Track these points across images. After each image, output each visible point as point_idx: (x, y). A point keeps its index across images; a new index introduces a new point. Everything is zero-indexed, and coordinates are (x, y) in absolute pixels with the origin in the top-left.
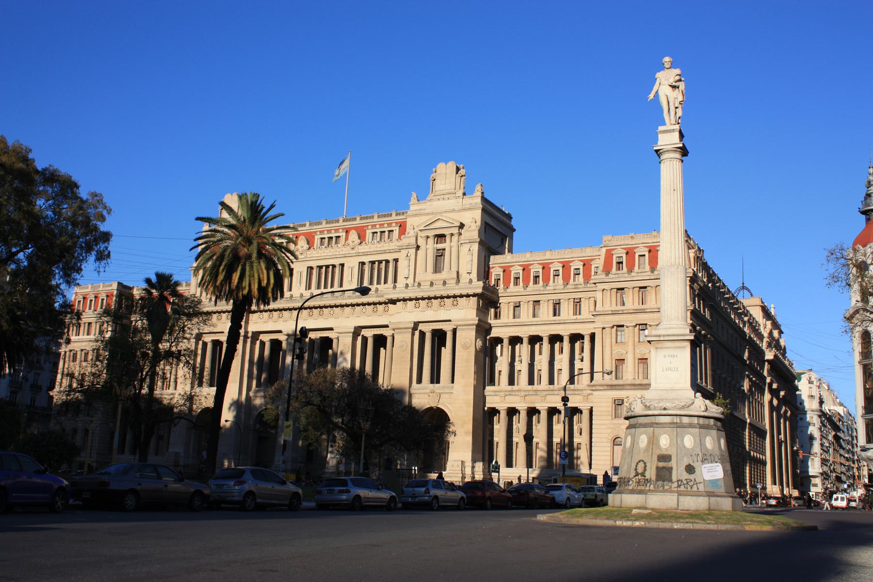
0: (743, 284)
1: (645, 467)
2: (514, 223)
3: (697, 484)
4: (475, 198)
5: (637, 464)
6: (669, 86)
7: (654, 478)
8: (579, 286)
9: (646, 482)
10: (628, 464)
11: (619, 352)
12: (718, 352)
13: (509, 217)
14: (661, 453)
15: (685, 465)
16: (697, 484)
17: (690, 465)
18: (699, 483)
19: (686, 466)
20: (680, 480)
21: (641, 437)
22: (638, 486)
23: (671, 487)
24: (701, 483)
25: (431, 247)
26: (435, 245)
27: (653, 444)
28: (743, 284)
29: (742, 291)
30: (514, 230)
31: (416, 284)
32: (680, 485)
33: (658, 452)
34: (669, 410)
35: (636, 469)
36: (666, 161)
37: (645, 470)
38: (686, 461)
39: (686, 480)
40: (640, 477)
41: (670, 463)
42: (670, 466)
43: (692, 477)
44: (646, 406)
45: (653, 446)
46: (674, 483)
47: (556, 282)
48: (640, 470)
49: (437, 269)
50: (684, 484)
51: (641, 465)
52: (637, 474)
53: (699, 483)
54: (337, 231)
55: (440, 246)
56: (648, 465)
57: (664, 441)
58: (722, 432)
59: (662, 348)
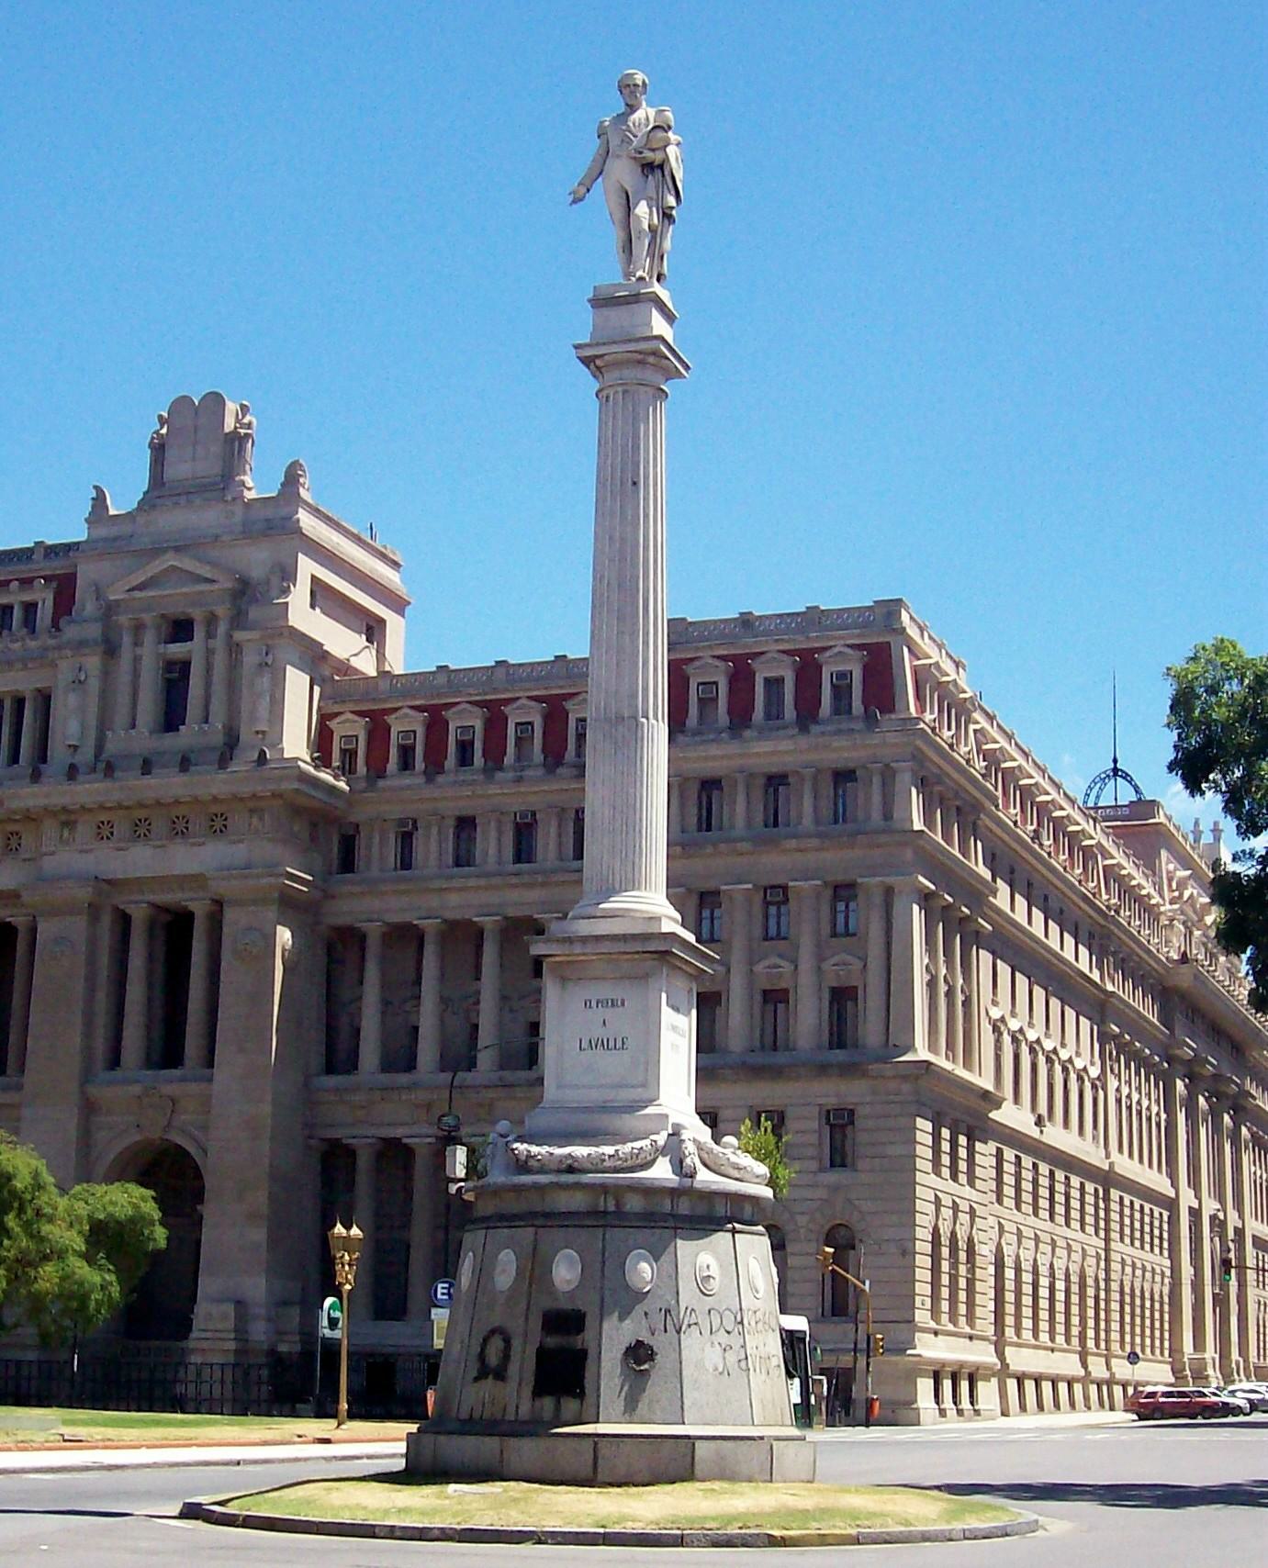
0: (1115, 761)
5: (486, 1340)
6: (574, 206)
10: (462, 1342)
11: (772, 969)
17: (640, 1343)
21: (500, 1257)
25: (151, 653)
26: (161, 648)
28: (1115, 761)
29: (1113, 781)
31: (102, 766)
33: (548, 1304)
35: (482, 1357)
37: (506, 1356)
48: (493, 1359)
49: (172, 718)
51: (496, 1344)
54: (27, 582)
55: (177, 650)
56: (516, 1343)
57: (565, 1272)
58: (762, 1238)
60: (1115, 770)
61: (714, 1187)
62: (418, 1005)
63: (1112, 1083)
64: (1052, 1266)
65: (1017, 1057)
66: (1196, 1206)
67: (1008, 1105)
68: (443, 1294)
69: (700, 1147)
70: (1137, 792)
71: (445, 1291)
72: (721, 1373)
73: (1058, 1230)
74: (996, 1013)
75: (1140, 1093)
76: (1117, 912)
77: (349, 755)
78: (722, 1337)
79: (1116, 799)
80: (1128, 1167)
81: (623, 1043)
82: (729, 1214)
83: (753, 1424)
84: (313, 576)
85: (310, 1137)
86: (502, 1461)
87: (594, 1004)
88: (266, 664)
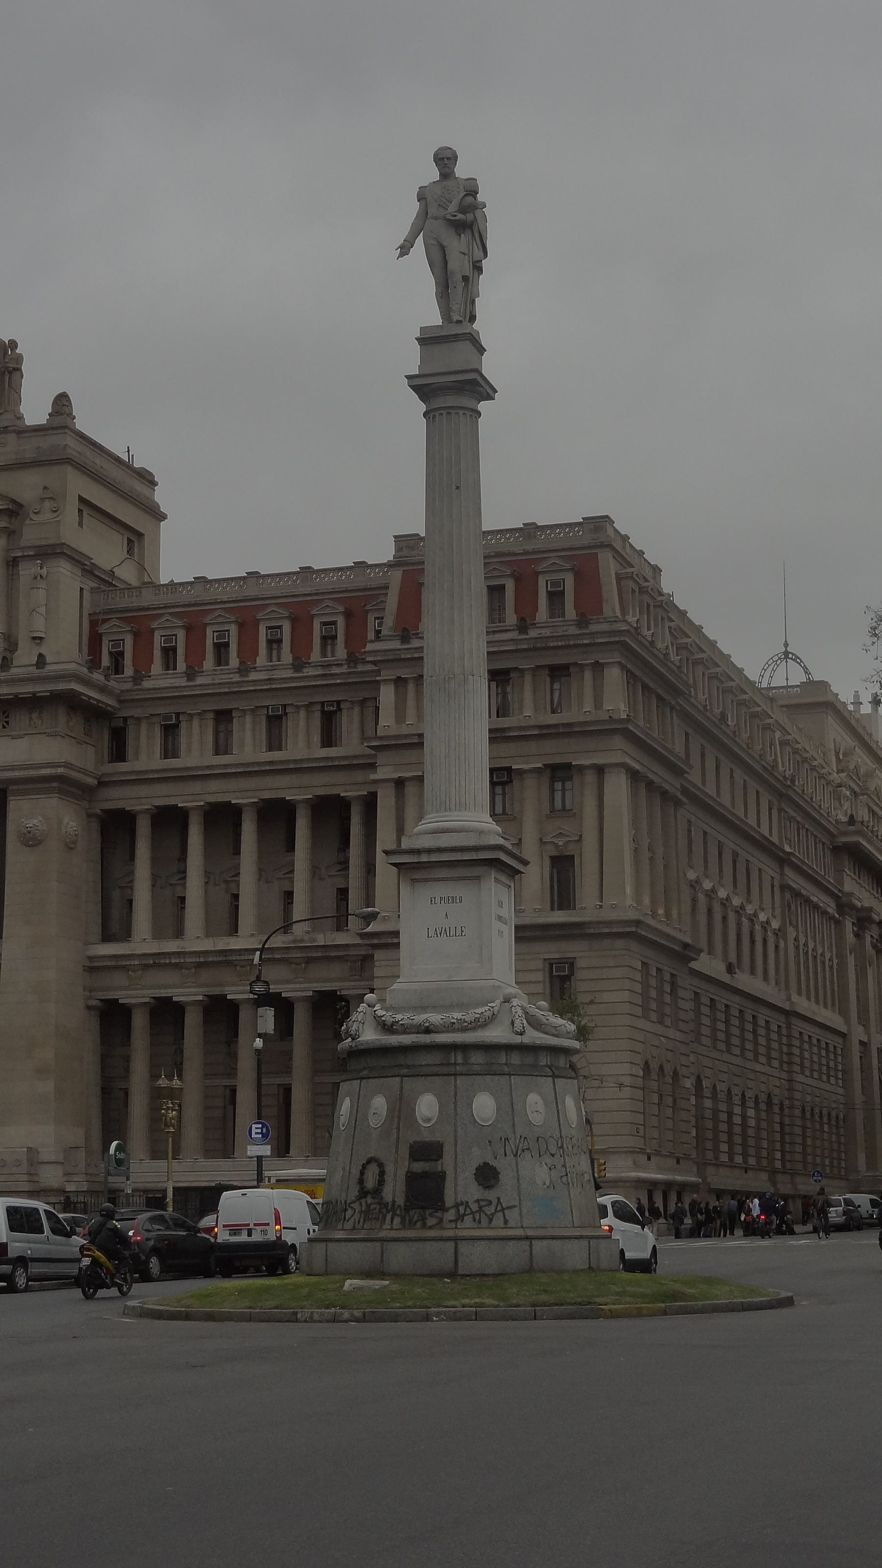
0: (786, 645)
1: (382, 1173)
2: (161, 497)
3: (503, 1210)
4: (50, 432)
5: (364, 1167)
7: (400, 1201)
8: (335, 670)
9: (384, 1211)
10: (343, 1169)
12: (705, 833)
13: (147, 479)
14: (418, 1139)
15: (476, 1165)
16: (503, 1210)
17: (486, 1164)
18: (508, 1208)
19: (477, 1169)
20: (462, 1203)
22: (364, 1221)
23: (441, 1220)
24: (515, 1206)
27: (399, 1118)
28: (786, 645)
30: (163, 517)
32: (464, 1215)
34: (438, 1032)
35: (361, 1181)
36: (437, 414)
37: (381, 1182)
38: (477, 1157)
39: (478, 1201)
40: (369, 1200)
41: (440, 1162)
42: (440, 1169)
43: (492, 1195)
44: (385, 1025)
45: (399, 1124)
46: (447, 1210)
47: (274, 658)
50: (472, 1213)
51: (373, 1170)
52: (363, 1193)
53: (508, 1208)
56: (390, 1169)
59: (426, 880)
60: (786, 654)
61: (538, 1042)
62: (184, 878)
63: (791, 933)
64: (743, 1095)
65: (725, 919)
66: (865, 1040)
67: (704, 956)
68: (256, 1133)
69: (523, 1009)
70: (806, 672)
71: (260, 1131)
72: (548, 1187)
73: (749, 1065)
74: (692, 875)
75: (815, 942)
76: (793, 781)
77: (117, 657)
78: (548, 1160)
79: (787, 679)
80: (803, 1005)
81: (462, 931)
82: (549, 1063)
83: (574, 1227)
84: (79, 495)
85: (90, 998)
86: (382, 1261)
87: (438, 900)
88: (41, 576)
